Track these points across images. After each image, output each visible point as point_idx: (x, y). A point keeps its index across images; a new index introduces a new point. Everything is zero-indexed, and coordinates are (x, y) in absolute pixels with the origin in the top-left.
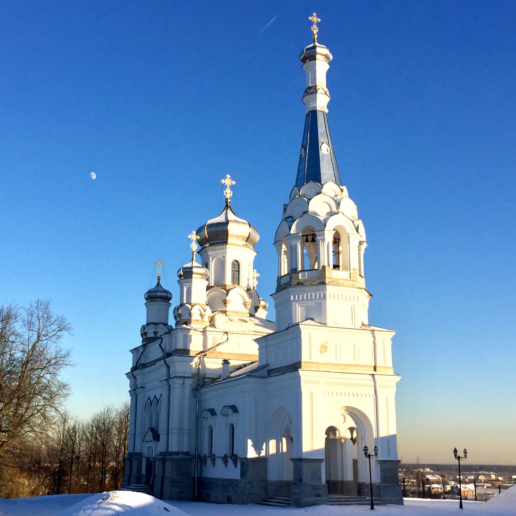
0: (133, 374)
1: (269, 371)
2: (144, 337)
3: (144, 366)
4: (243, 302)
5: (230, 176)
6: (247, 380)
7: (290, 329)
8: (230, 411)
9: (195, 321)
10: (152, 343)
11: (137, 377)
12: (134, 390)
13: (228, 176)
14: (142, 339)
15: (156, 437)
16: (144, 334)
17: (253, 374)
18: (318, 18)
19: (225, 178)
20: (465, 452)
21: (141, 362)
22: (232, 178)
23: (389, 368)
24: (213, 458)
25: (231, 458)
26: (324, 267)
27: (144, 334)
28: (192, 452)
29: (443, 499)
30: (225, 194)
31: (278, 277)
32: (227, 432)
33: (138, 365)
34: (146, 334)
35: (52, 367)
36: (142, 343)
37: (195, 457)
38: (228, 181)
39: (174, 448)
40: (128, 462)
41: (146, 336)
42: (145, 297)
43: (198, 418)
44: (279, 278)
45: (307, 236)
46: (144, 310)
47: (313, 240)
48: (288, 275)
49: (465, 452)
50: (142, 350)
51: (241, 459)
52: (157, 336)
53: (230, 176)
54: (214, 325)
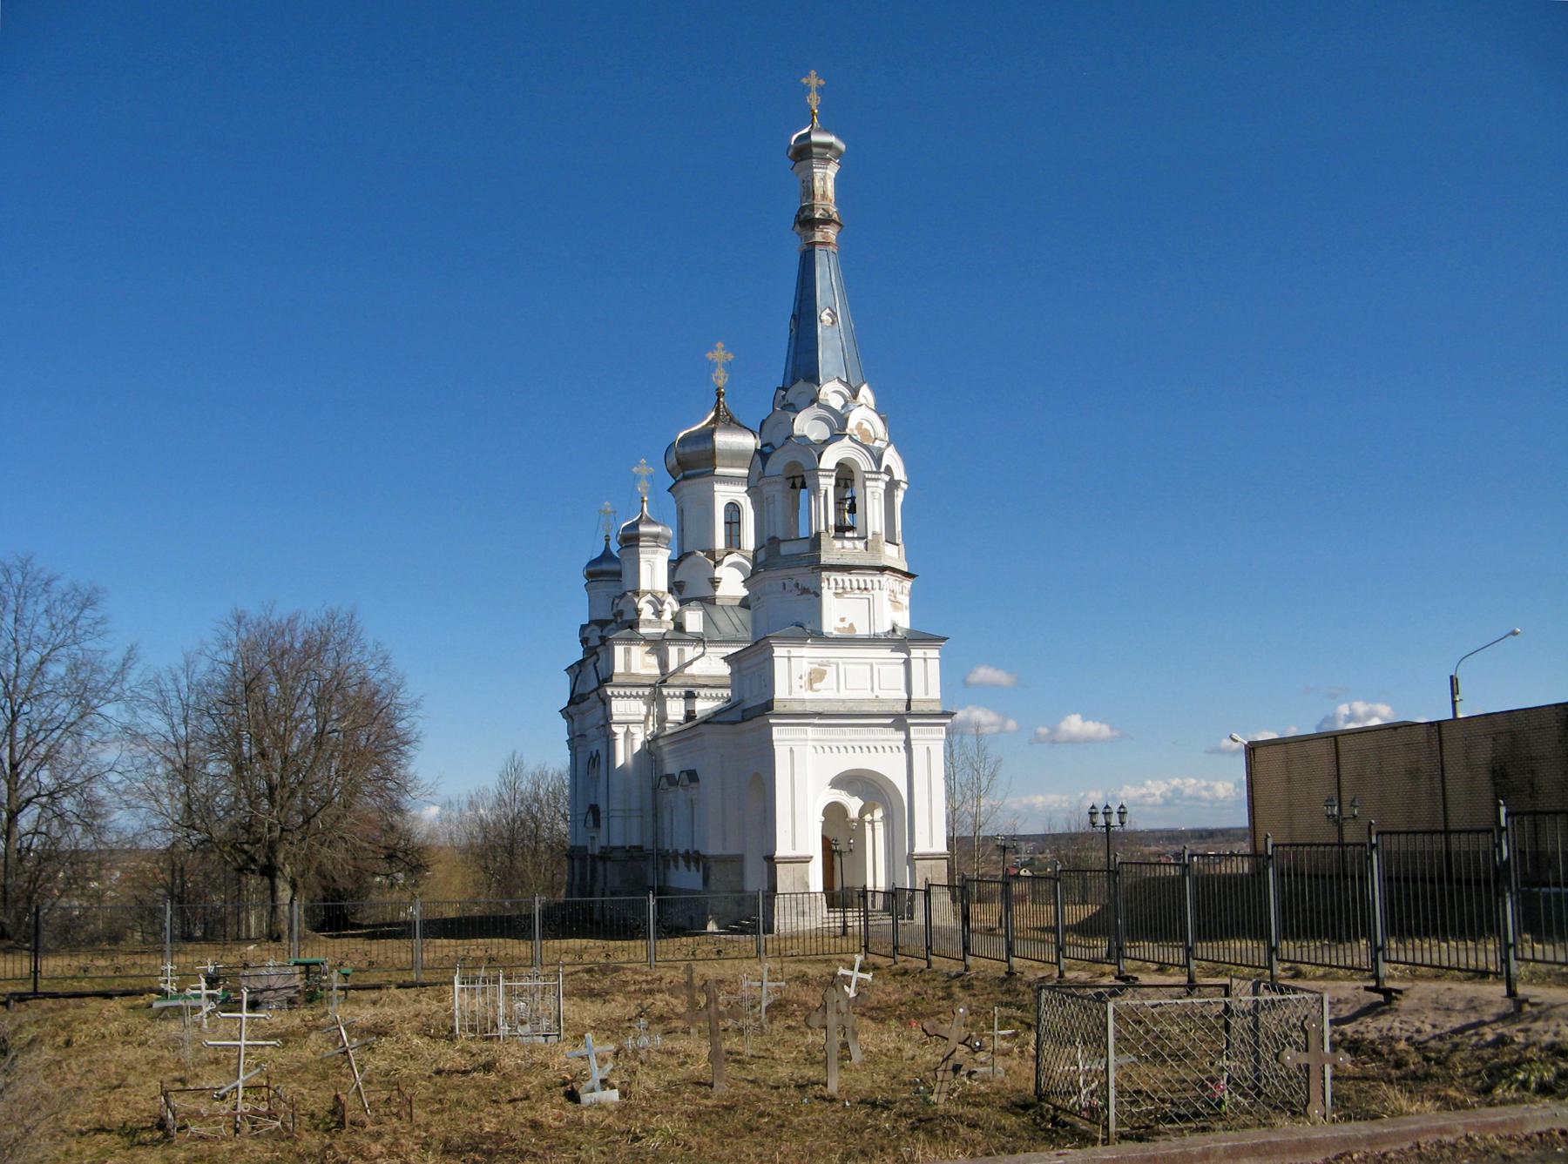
1: (744, 711)
13: (720, 345)
16: (584, 641)
22: (727, 349)
26: (818, 534)
28: (648, 846)
38: (719, 354)
39: (617, 842)
43: (655, 788)
45: (793, 477)
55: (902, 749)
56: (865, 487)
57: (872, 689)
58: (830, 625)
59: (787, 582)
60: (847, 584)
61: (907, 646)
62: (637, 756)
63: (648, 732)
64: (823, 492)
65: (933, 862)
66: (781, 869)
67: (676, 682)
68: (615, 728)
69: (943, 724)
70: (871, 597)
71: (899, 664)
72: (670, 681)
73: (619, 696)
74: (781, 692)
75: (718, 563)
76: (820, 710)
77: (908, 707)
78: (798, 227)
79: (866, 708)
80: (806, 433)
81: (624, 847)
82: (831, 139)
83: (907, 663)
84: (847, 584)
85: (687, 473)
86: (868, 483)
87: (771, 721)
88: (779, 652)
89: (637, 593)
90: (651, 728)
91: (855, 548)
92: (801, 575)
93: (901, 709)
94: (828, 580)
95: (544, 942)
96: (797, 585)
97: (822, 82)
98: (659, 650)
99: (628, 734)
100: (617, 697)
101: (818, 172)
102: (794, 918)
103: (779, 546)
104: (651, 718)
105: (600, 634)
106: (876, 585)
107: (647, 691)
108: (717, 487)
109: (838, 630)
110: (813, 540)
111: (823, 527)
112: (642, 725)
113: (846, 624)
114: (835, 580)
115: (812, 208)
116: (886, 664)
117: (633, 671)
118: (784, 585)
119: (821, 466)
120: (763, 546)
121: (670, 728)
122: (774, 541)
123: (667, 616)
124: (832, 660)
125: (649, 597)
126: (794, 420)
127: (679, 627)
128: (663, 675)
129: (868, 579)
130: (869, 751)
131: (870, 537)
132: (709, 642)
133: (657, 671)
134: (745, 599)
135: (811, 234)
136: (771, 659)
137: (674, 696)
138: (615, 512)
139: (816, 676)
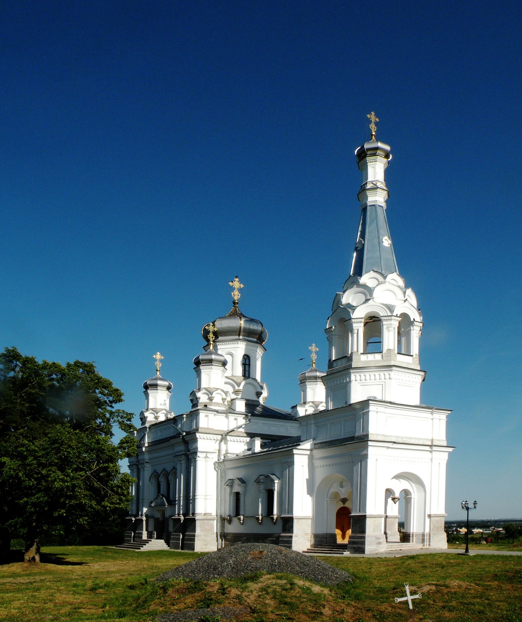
14: (141, 422)
18: (376, 117)
20: (475, 503)
23: (443, 441)
29: (424, 537)
30: (233, 296)
49: (475, 503)
65: (438, 518)
67: (233, 435)
70: (383, 383)
119: (353, 318)
131: (384, 351)
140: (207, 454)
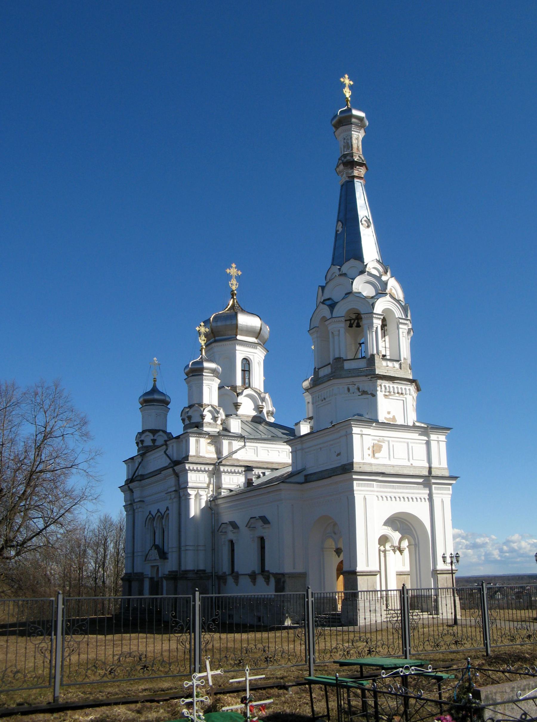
0: (129, 487)
1: (306, 476)
2: (140, 445)
3: (143, 477)
4: (253, 407)
5: (235, 266)
6: (283, 486)
7: (336, 427)
8: (260, 523)
9: (208, 425)
10: (153, 452)
11: (134, 490)
12: (130, 504)
13: (234, 265)
15: (163, 555)
16: (140, 442)
17: (287, 481)
18: (344, 82)
19: (230, 267)
21: (138, 473)
22: (238, 268)
24: (236, 576)
25: (262, 575)
26: (373, 356)
27: (140, 443)
28: (209, 570)
31: (315, 368)
32: (255, 546)
33: (135, 476)
34: (142, 441)
35: (61, 465)
36: (138, 452)
37: (212, 575)
38: (233, 271)
40: (413, 599)
41: (142, 444)
42: (140, 401)
43: (213, 532)
44: (317, 370)
46: (139, 414)
47: (358, 326)
48: (330, 365)
50: (140, 460)
51: (275, 575)
52: (155, 444)
53: (235, 266)
54: (228, 429)
55: (427, 500)
56: (398, 328)
57: (409, 460)
58: (382, 417)
59: (350, 386)
60: (392, 390)
61: (427, 432)
62: (203, 510)
63: (209, 495)
64: (375, 329)
66: (361, 580)
67: (228, 464)
68: (190, 491)
69: (450, 484)
70: (404, 399)
71: (422, 443)
72: (223, 463)
73: (193, 470)
74: (357, 458)
75: (238, 395)
76: (383, 471)
77: (430, 471)
78: (341, 167)
79: (406, 472)
80: (360, 291)
81: (194, 571)
82: (362, 114)
83: (428, 443)
84: (392, 390)
85: (217, 338)
86: (401, 326)
87: (354, 477)
88: (356, 430)
89: (201, 405)
90: (211, 493)
91: (394, 367)
92: (363, 383)
93: (426, 473)
94: (381, 385)
95: (68, 637)
96: (358, 389)
97: (352, 83)
98: (216, 442)
99: (197, 496)
100: (191, 471)
101: (355, 134)
102: (368, 614)
103: (343, 363)
104: (211, 486)
105: (152, 438)
106: (408, 392)
107: (211, 468)
108: (238, 347)
109: (385, 418)
110: (369, 359)
111: (375, 352)
112: (207, 490)
113: (391, 416)
114: (385, 386)
115: (351, 155)
116: (416, 443)
117: (201, 455)
118: (349, 389)
119: (375, 312)
120: (329, 364)
121: (224, 493)
122: (339, 360)
123: (219, 422)
124: (385, 438)
125: (210, 408)
126: (352, 282)
127: (226, 429)
128: (219, 459)
129: (403, 387)
130: (387, 500)
131: (402, 361)
132: (248, 439)
133: (215, 456)
134: (254, 417)
135: (350, 171)
136: (351, 434)
137: (228, 472)
138: (159, 364)
139: (376, 449)
140: (198, 490)
